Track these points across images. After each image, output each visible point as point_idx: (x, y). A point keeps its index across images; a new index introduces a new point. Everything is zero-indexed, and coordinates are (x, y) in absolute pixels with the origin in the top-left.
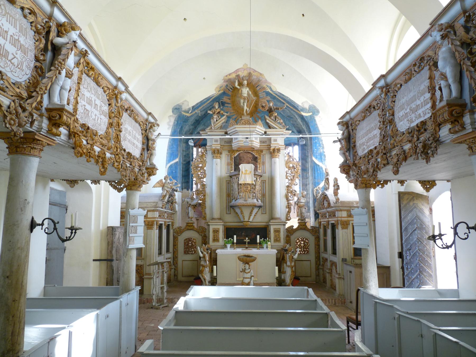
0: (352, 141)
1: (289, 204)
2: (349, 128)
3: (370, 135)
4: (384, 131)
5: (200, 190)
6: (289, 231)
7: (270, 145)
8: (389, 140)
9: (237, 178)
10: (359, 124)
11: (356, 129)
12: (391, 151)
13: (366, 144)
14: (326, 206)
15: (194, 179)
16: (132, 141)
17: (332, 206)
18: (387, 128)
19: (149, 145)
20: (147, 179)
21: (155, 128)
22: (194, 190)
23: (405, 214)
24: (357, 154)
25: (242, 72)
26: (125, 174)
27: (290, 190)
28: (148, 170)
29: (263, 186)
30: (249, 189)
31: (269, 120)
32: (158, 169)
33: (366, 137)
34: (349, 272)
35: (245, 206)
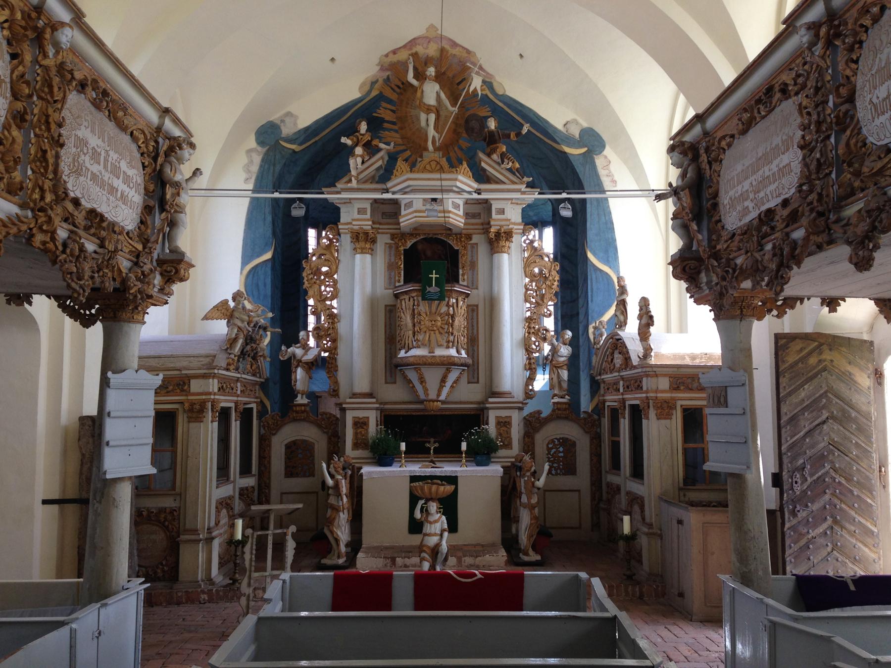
0: (706, 194)
1: (532, 361)
2: (701, 159)
3: (766, 169)
4: (821, 151)
5: (324, 327)
6: (530, 423)
7: (489, 223)
8: (833, 176)
9: (412, 300)
10: (729, 145)
11: (721, 161)
12: (842, 207)
13: (751, 196)
14: (618, 366)
15: (311, 302)
16: (106, 178)
17: (634, 364)
18: (828, 142)
19: (165, 198)
20: (161, 290)
21: (186, 152)
22: (310, 328)
23: (791, 386)
24: (723, 227)
25: (425, 45)
26: (75, 270)
27: (534, 328)
28: (165, 267)
29: (472, 319)
30: (439, 324)
31: (487, 163)
32: (193, 266)
33: (752, 178)
34: (675, 522)
35: (429, 364)
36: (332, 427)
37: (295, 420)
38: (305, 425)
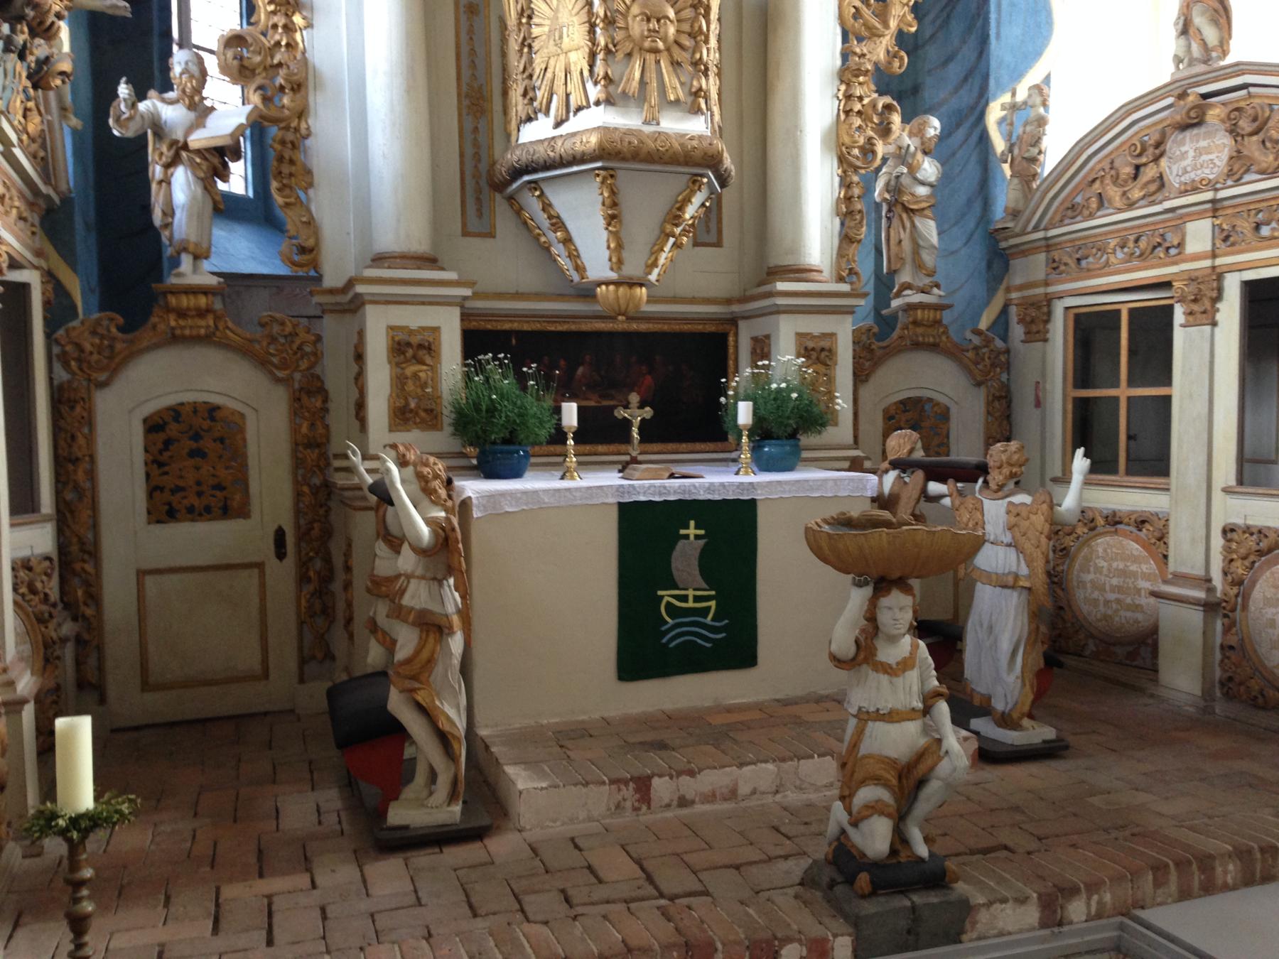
36: (304, 364)
37: (175, 339)
38: (213, 356)
